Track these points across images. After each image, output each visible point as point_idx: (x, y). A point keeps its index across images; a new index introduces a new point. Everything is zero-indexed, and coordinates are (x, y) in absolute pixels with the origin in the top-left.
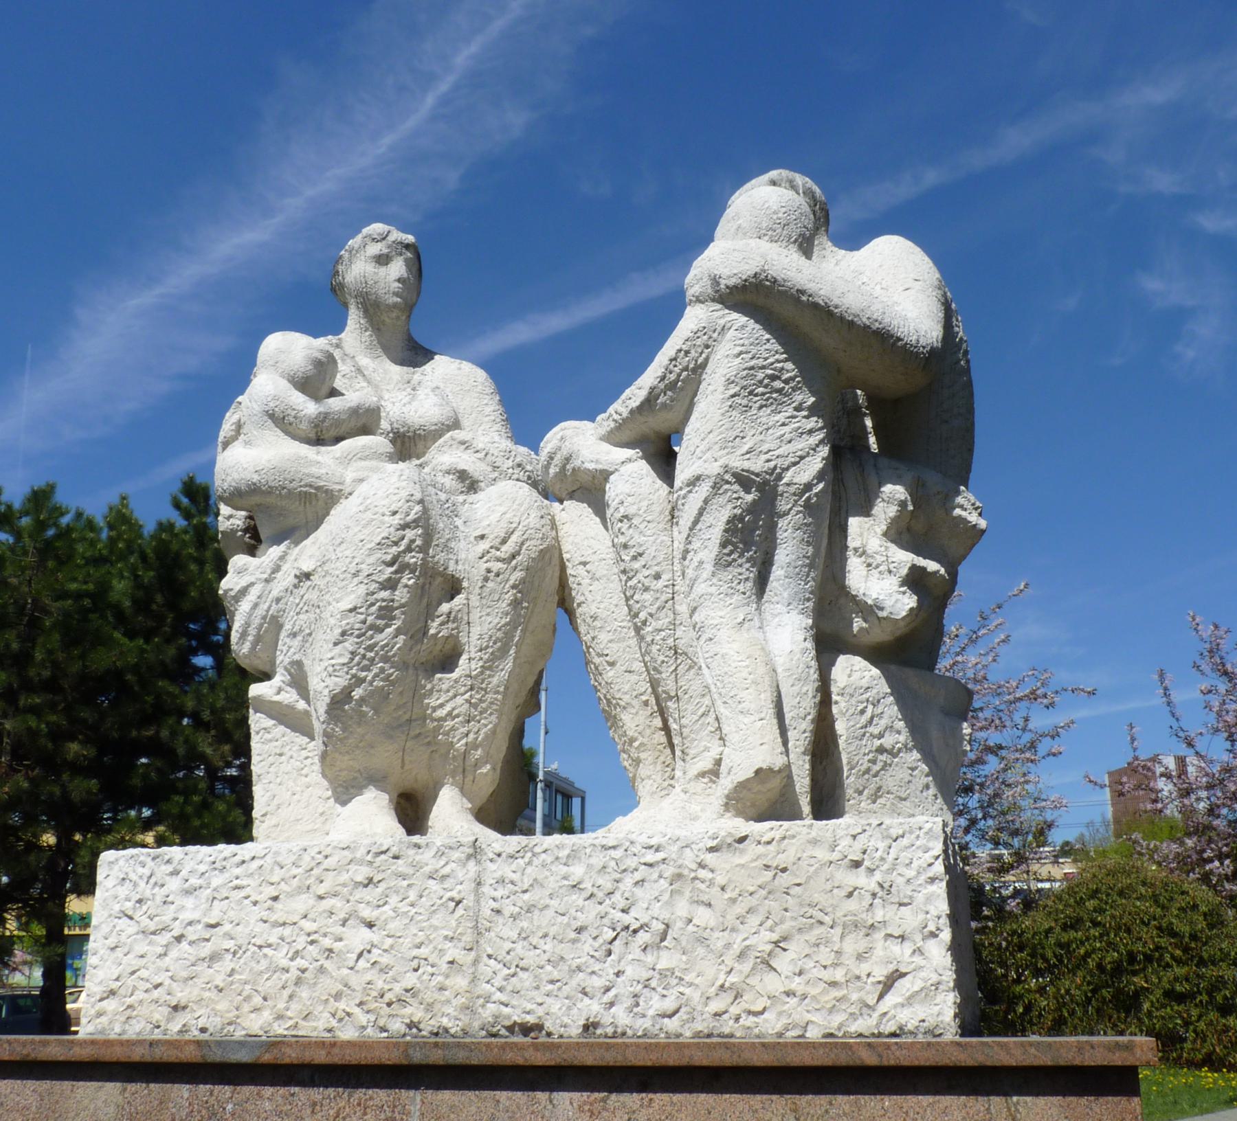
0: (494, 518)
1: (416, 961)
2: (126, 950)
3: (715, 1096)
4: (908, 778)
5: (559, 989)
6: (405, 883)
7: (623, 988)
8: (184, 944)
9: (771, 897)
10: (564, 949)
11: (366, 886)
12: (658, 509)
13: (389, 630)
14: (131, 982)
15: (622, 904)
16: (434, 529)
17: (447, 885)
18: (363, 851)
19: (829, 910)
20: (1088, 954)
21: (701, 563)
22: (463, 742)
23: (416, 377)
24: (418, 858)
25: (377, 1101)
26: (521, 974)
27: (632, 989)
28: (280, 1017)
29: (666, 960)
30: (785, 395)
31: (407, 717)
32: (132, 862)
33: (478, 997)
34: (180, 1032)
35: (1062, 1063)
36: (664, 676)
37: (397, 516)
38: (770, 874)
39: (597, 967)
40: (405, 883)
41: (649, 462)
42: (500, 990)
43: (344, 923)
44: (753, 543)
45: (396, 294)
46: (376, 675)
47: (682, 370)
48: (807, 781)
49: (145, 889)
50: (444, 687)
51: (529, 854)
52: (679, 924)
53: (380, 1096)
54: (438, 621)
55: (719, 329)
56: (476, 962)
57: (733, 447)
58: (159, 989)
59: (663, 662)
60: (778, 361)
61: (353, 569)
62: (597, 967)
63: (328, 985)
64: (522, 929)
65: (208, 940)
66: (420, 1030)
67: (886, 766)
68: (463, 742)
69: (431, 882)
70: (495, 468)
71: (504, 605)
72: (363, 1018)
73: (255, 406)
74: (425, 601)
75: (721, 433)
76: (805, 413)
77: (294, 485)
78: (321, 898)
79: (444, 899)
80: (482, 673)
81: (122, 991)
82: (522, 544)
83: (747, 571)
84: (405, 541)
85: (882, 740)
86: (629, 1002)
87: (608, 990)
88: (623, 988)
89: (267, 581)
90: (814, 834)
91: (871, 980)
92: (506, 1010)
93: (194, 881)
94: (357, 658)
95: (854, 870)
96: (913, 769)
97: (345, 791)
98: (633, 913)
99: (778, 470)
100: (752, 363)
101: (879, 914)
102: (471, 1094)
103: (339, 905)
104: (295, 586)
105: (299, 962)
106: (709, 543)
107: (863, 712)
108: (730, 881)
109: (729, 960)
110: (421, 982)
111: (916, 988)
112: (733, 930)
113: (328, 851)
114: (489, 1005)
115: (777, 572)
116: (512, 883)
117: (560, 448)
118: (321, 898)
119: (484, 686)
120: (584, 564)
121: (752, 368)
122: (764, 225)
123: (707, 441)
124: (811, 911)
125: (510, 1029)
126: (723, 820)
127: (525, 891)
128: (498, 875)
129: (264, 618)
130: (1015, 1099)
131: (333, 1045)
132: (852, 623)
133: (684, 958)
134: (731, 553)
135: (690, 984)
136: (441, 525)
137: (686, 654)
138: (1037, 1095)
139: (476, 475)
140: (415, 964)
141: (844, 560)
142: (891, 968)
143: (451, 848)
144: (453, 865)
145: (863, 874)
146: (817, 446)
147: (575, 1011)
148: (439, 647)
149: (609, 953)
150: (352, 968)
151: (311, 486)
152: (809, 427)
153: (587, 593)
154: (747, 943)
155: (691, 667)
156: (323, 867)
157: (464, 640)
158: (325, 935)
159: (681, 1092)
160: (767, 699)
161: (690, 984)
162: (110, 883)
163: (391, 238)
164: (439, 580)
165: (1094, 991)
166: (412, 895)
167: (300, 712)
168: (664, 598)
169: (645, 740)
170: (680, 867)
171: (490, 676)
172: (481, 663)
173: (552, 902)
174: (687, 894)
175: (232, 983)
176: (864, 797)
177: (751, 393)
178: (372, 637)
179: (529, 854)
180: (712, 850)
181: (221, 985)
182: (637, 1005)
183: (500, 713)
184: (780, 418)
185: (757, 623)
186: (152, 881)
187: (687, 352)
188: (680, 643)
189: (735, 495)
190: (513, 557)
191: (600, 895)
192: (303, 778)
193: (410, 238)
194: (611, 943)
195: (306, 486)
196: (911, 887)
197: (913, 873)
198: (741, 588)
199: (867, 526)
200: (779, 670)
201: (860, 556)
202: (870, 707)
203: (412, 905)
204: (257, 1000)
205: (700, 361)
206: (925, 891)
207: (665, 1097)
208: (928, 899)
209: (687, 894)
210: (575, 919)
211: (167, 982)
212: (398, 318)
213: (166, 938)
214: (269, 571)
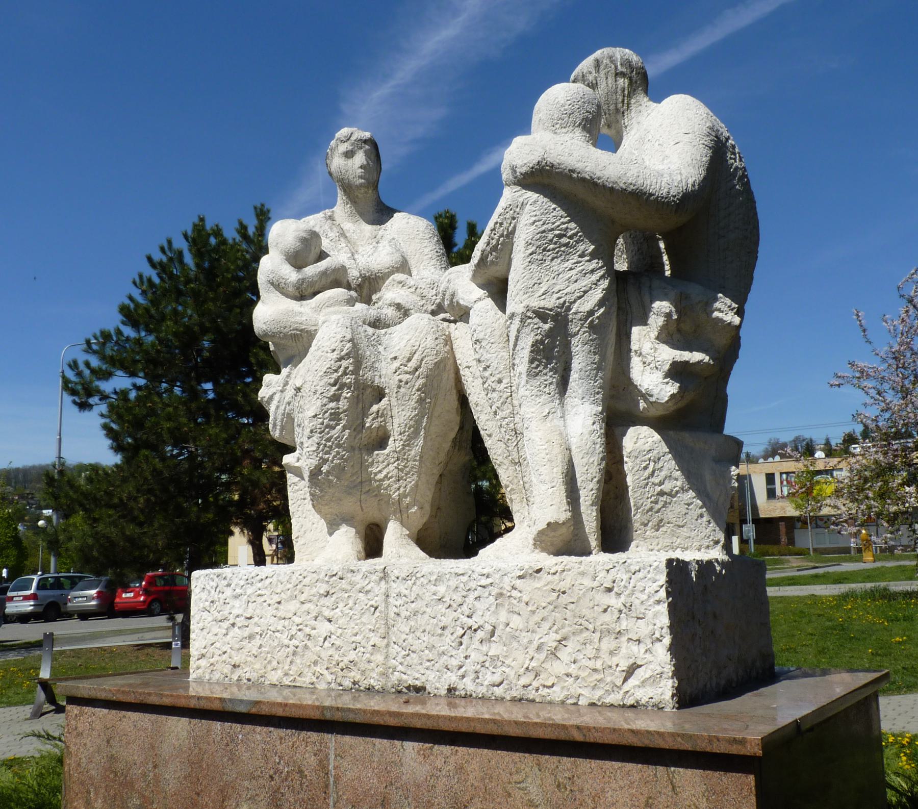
4: (685, 511)
6: (347, 595)
7: (469, 667)
10: (435, 640)
11: (326, 596)
12: (499, 333)
13: (338, 427)
14: (211, 649)
15: (467, 613)
16: (363, 357)
18: (323, 574)
19: (591, 621)
21: (520, 374)
22: (397, 493)
23: (380, 233)
24: (353, 579)
25: (312, 739)
26: (412, 654)
28: (286, 674)
29: (495, 649)
31: (359, 480)
37: (335, 353)
40: (347, 595)
42: (401, 664)
43: (316, 618)
45: (360, 177)
46: (335, 456)
47: (500, 237)
49: (215, 595)
50: (380, 459)
51: (414, 578)
52: (501, 627)
53: (314, 736)
54: (371, 417)
56: (387, 646)
60: (563, 223)
62: (454, 652)
63: (310, 656)
67: (665, 504)
68: (397, 493)
69: (361, 594)
70: (423, 297)
71: (413, 403)
72: (329, 678)
74: (360, 405)
76: (587, 258)
77: (287, 330)
80: (403, 449)
81: (208, 655)
82: (422, 360)
83: (550, 377)
84: (342, 368)
85: (662, 487)
86: (473, 676)
87: (461, 667)
88: (469, 667)
89: (282, 391)
90: (582, 569)
91: (619, 669)
92: (405, 677)
93: (238, 591)
96: (689, 505)
97: (332, 527)
98: (474, 618)
99: (567, 304)
100: (543, 228)
101: (624, 625)
102: (360, 739)
103: (312, 607)
104: (296, 395)
106: (523, 360)
107: (646, 468)
108: (531, 599)
111: (647, 676)
112: (533, 632)
113: (305, 574)
115: (574, 376)
116: (405, 596)
117: (448, 288)
120: (469, 367)
121: (544, 232)
125: (408, 688)
127: (413, 602)
128: (397, 591)
129: (283, 414)
130: (672, 769)
131: (286, 705)
133: (505, 649)
135: (509, 666)
136: (368, 353)
138: (687, 768)
139: (407, 306)
140: (354, 645)
142: (631, 661)
146: (598, 281)
147: (442, 680)
148: (374, 434)
149: (461, 644)
152: (591, 268)
154: (541, 641)
158: (306, 626)
159: (474, 747)
161: (509, 666)
163: (353, 138)
164: (370, 390)
168: (505, 396)
169: (514, 487)
172: (402, 443)
174: (506, 607)
175: (261, 653)
176: (648, 528)
177: (544, 250)
178: (328, 433)
179: (414, 578)
180: (520, 577)
182: (478, 678)
183: (419, 474)
184: (568, 264)
185: (559, 414)
187: (501, 224)
188: (519, 426)
189: (536, 326)
190: (416, 370)
191: (455, 605)
193: (367, 135)
196: (644, 607)
197: (645, 597)
198: (547, 390)
200: (573, 448)
202: (652, 464)
206: (653, 610)
208: (655, 615)
209: (506, 607)
212: (366, 192)
213: (226, 624)
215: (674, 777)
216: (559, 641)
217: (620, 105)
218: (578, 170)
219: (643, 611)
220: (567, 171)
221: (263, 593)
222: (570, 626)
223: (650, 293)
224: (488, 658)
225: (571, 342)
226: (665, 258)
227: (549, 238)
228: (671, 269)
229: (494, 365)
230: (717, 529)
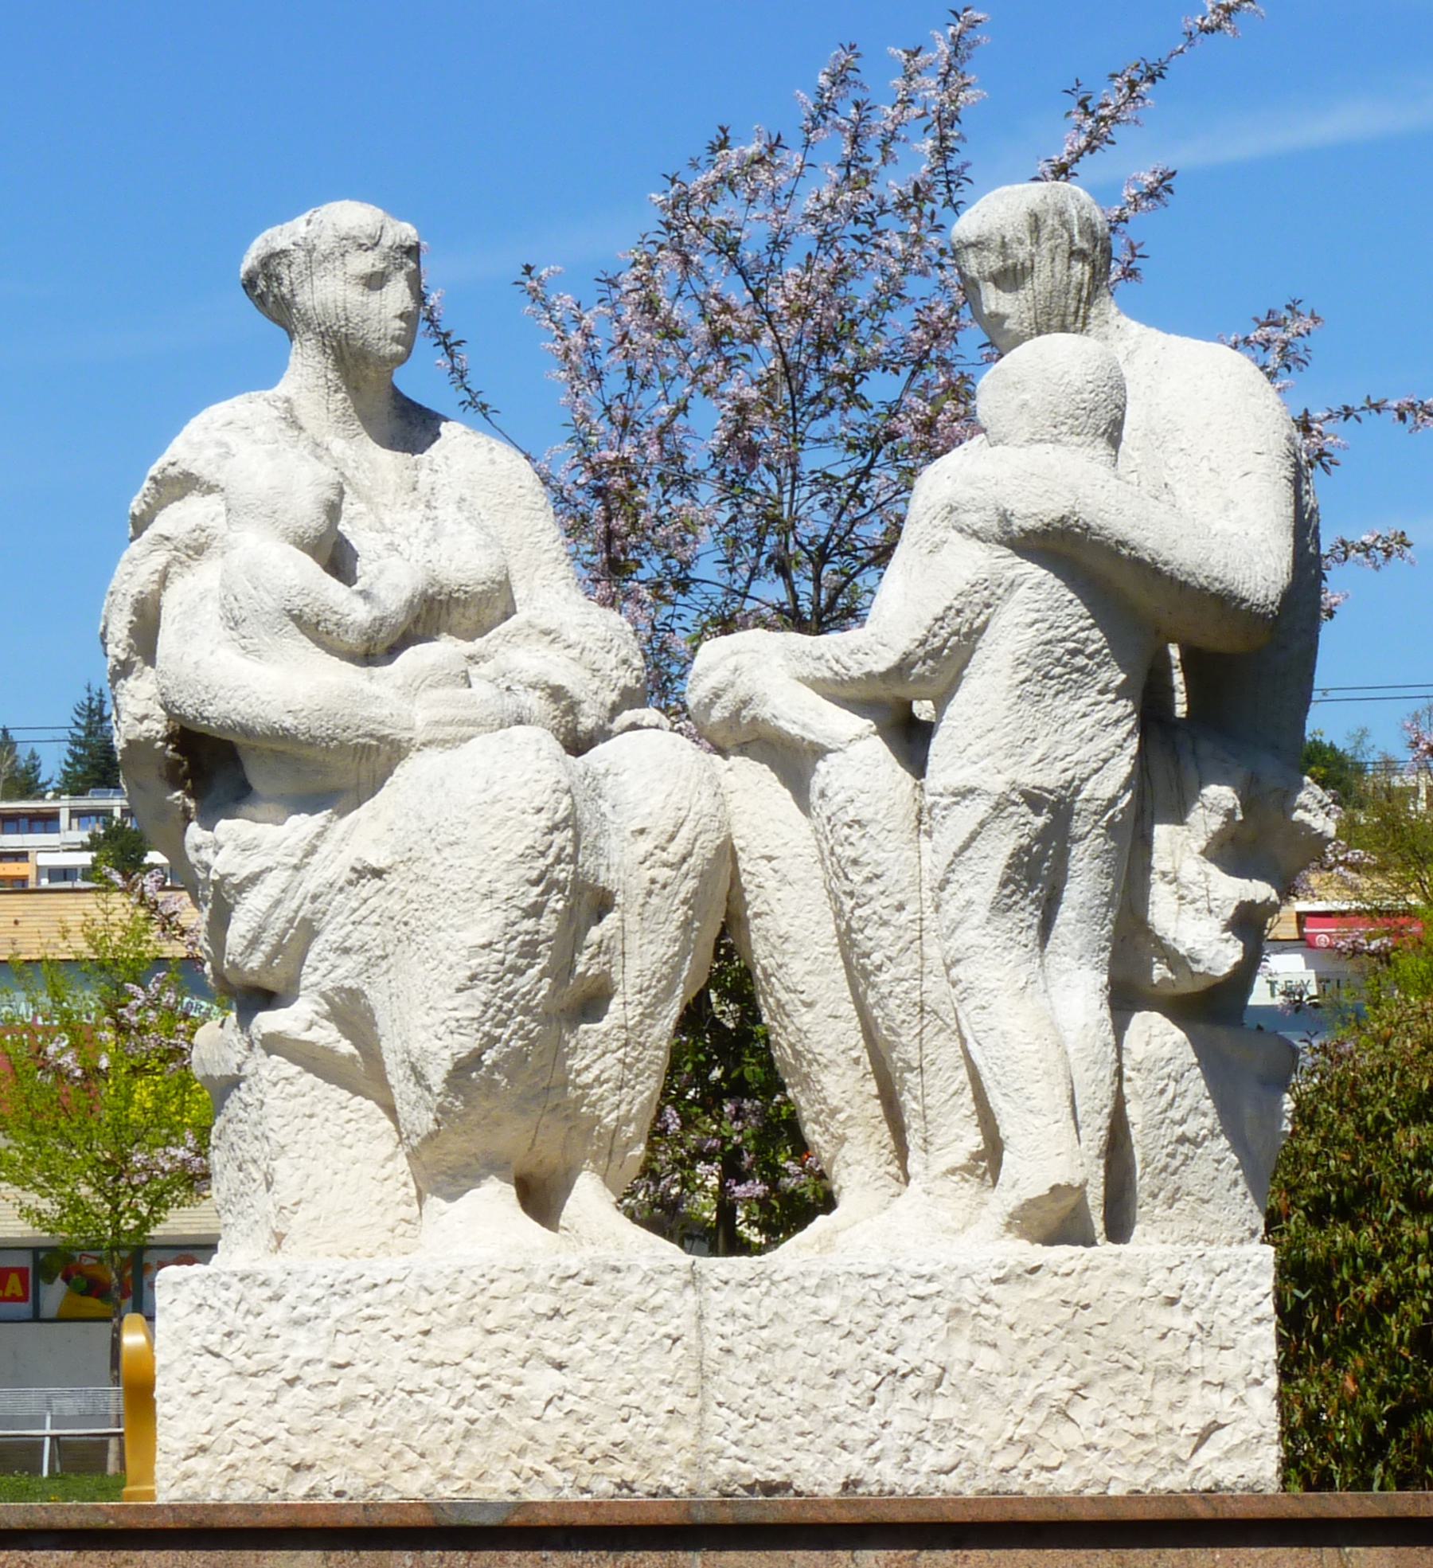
0: (656, 801)
1: (626, 1410)
2: (217, 1397)
3: (1036, 1552)
5: (812, 1442)
6: (604, 1315)
7: (890, 1440)
8: (299, 1389)
9: (1070, 1338)
10: (813, 1396)
11: (551, 1318)
12: (902, 812)
13: (533, 972)
14: (228, 1435)
15: (888, 1344)
17: (660, 1317)
20: (1387, 1302)
21: (970, 903)
22: (614, 1115)
24: (618, 1284)
26: (762, 1425)
27: (902, 1442)
28: (445, 1477)
29: (941, 1409)
30: (1088, 674)
31: (544, 1084)
32: (210, 1283)
33: (708, 1452)
34: (307, 1496)
35: (1397, 1514)
36: (904, 1040)
37: (544, 815)
38: (1069, 1311)
39: (858, 1417)
41: (887, 741)
42: (736, 1443)
44: (1039, 878)
45: (396, 340)
46: (515, 1033)
48: (1101, 1191)
50: (591, 1042)
52: (959, 1368)
54: (587, 954)
55: (1006, 584)
56: (702, 1410)
57: (1022, 755)
58: (270, 1444)
59: (904, 1022)
60: (1082, 629)
61: (482, 886)
62: (858, 1417)
63: (504, 1439)
64: (762, 1372)
65: (335, 1384)
66: (633, 1491)
68: (614, 1115)
69: (638, 1314)
71: (672, 929)
72: (558, 1478)
73: (267, 598)
75: (1006, 735)
76: (1111, 696)
78: (490, 1332)
79: (657, 1336)
80: (641, 1022)
82: (696, 840)
83: (1030, 915)
85: (1184, 1127)
87: (872, 1443)
88: (890, 1440)
89: (296, 868)
90: (1122, 1266)
91: (1185, 1431)
93: (305, 1309)
94: (491, 1011)
95: (1169, 1308)
96: (1219, 1162)
98: (901, 1354)
99: (1077, 782)
101: (1196, 1359)
103: (516, 1341)
104: (350, 883)
105: (465, 1411)
107: (1162, 1092)
108: (1020, 1318)
109: (1019, 1408)
110: (634, 1435)
111: (1236, 1441)
112: (1024, 1375)
113: (494, 1274)
114: (721, 1461)
115: (1066, 914)
116: (746, 1317)
118: (490, 1332)
119: (642, 1039)
120: (770, 859)
122: (1063, 409)
123: (984, 741)
124: (1117, 1355)
125: (750, 1489)
126: (1003, 1242)
128: (727, 1306)
129: (291, 921)
130: (1347, 1550)
132: (1151, 970)
133: (964, 1407)
134: (1013, 893)
135: (972, 1437)
137: (936, 1013)
138: (1370, 1545)
140: (624, 1413)
141: (1146, 886)
142: (1209, 1418)
143: (661, 1273)
144: (667, 1294)
145: (1180, 1313)
146: (1125, 740)
149: (873, 1401)
150: (538, 1419)
151: (372, 736)
152: (1115, 716)
153: (773, 902)
154: (1041, 1390)
155: (941, 1030)
156: (488, 1294)
157: (617, 977)
158: (499, 1378)
160: (1062, 1091)
161: (972, 1437)
162: (180, 1309)
164: (588, 894)
165: (1398, 1419)
166: (615, 1331)
167: (343, 1057)
168: (908, 936)
169: (854, 1112)
170: (958, 1301)
171: (651, 1026)
172: (640, 1010)
173: (799, 1341)
174: (967, 1332)
175: (375, 1437)
176: (1158, 1202)
177: (1045, 677)
178: (511, 982)
179: (766, 1283)
180: (998, 1281)
181: (360, 1439)
182: (908, 1460)
184: (1080, 706)
185: (1041, 985)
186: (243, 1307)
187: (959, 612)
189: (1022, 820)
190: (684, 859)
192: (346, 1150)
194: (874, 1390)
195: (365, 735)
198: (1022, 938)
199: (1180, 839)
200: (1071, 1050)
201: (1170, 883)
202: (1172, 1084)
203: (616, 1342)
204: (411, 1457)
205: (977, 623)
206: (1251, 1334)
207: (982, 1553)
208: (1254, 1342)
209: (967, 1332)
210: (829, 1361)
211: (284, 1436)
213: (275, 1381)
214: (300, 854)
215: (1349, 1561)
216: (1075, 1391)
217: (1071, 319)
218: (1133, 544)
219: (1233, 1336)
220: (1112, 542)
221: (380, 1312)
222: (1095, 1362)
223: (1197, 766)
224: (930, 1425)
225: (1070, 850)
226: (1178, 678)
227: (1056, 655)
228: (1189, 701)
229: (893, 873)
230: (1256, 1208)
